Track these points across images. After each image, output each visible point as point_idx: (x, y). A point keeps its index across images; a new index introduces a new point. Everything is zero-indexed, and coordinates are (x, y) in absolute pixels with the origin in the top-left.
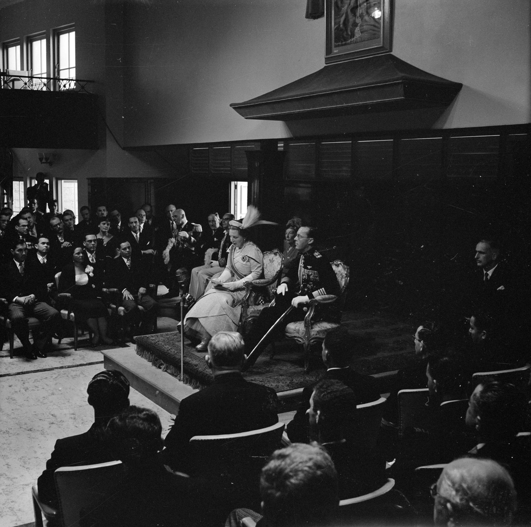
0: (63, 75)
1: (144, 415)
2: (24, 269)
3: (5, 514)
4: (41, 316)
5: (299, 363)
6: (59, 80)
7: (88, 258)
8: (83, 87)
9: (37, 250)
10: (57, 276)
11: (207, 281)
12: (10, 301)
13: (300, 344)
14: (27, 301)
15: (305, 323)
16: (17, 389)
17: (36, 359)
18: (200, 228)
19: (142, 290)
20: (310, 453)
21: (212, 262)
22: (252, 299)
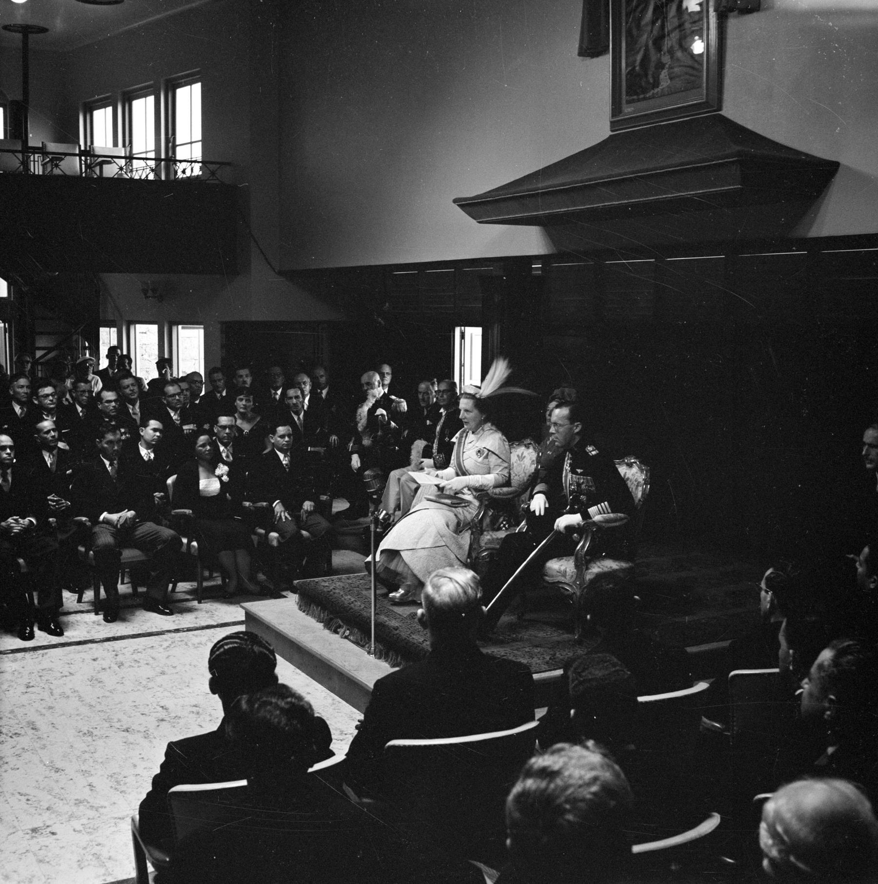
0: (182, 153)
2: (118, 471)
4: (147, 544)
6: (175, 161)
10: (170, 481)
12: (95, 521)
14: (122, 521)
16: (105, 664)
18: (404, 406)
19: (308, 505)
22: (487, 521)
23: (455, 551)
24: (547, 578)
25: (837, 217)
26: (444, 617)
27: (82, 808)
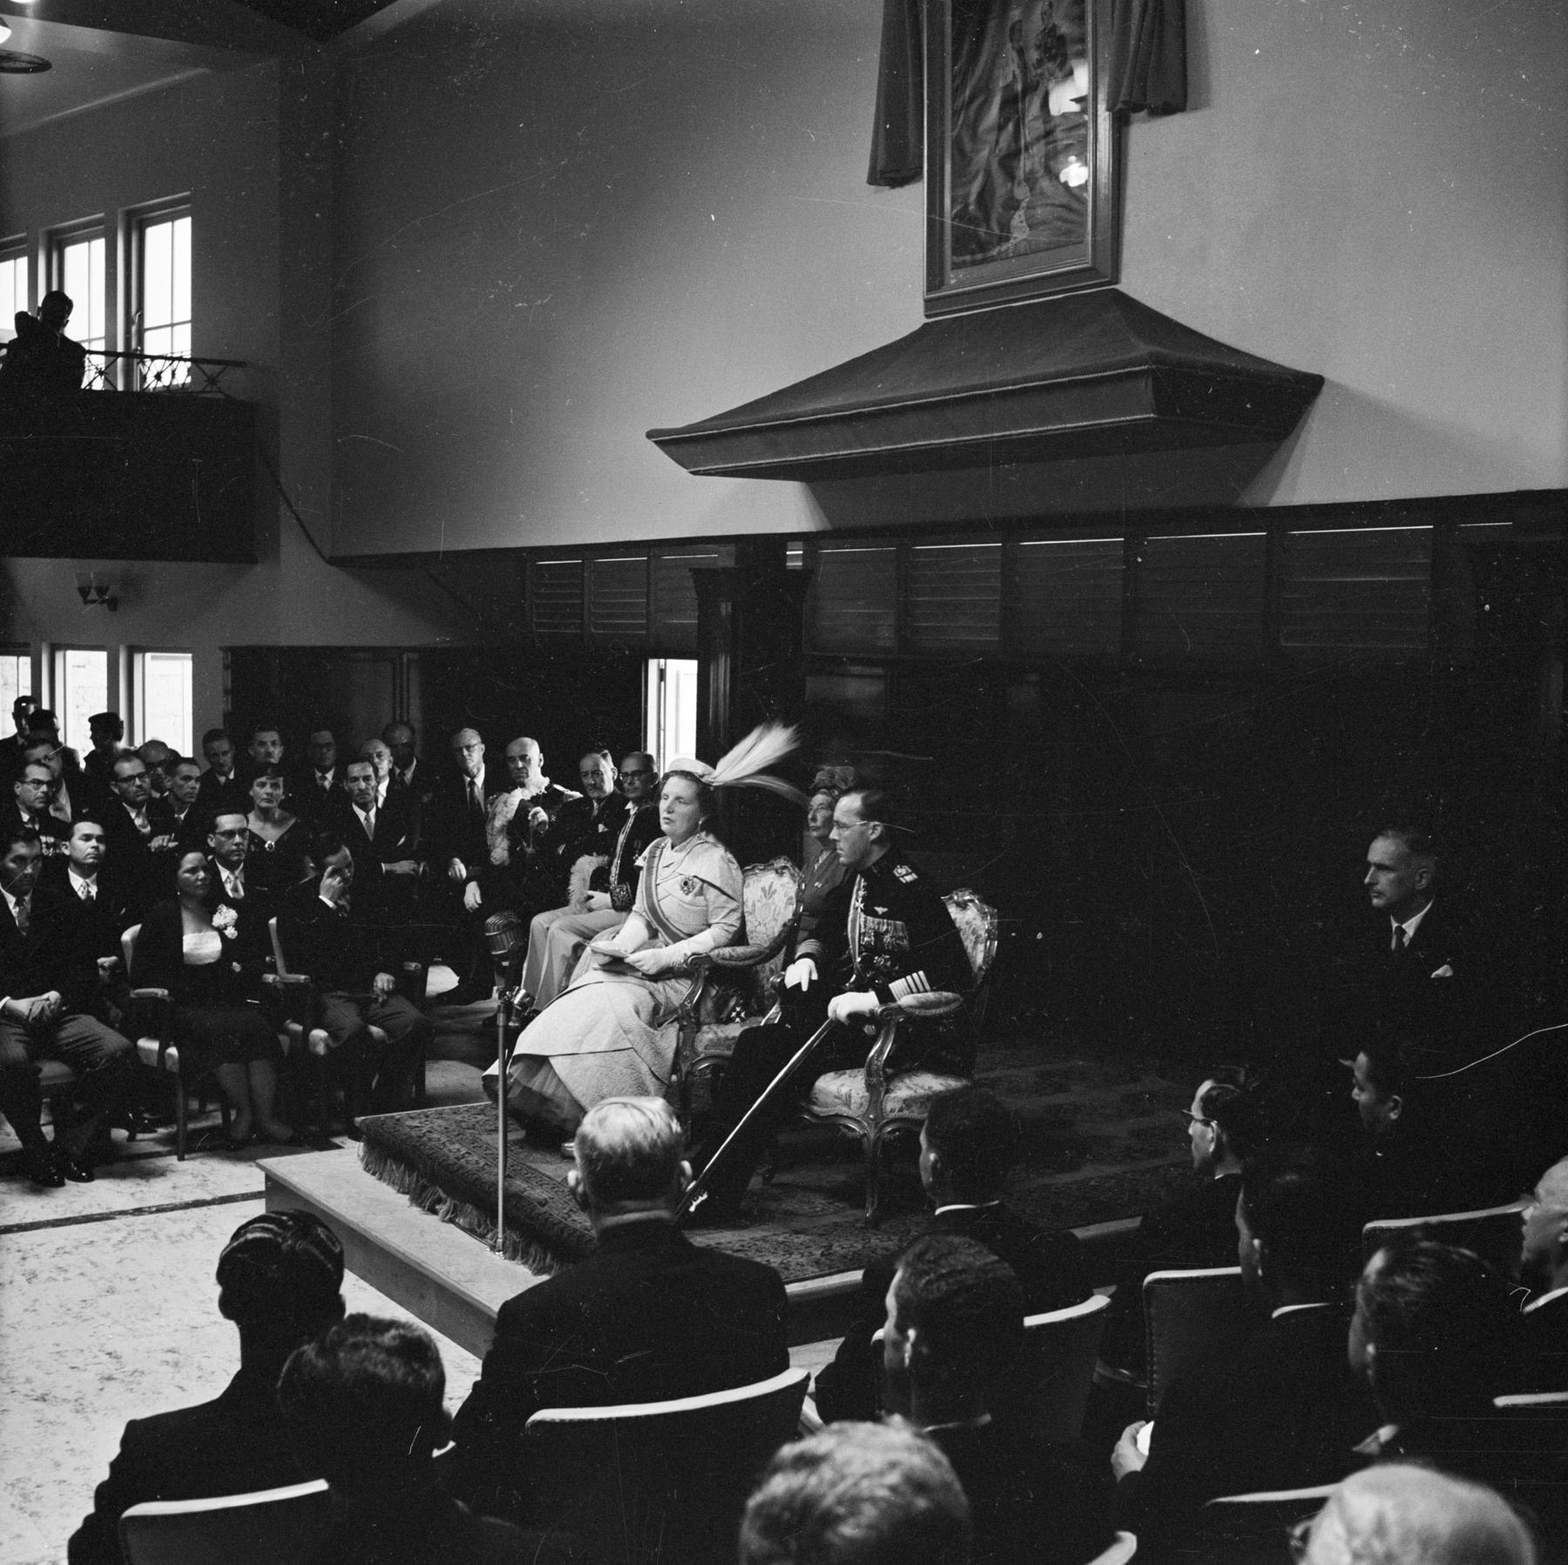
0: (154, 343)
1: (394, 1338)
4: (78, 1055)
5: (849, 1195)
6: (142, 357)
7: (221, 885)
8: (212, 380)
9: (66, 861)
10: (127, 936)
11: (578, 949)
13: (854, 1139)
14: (36, 1010)
15: (869, 1074)
17: (62, 1184)
19: (383, 981)
20: (890, 1448)
21: (591, 897)
22: (709, 1004)
26: (619, 1174)
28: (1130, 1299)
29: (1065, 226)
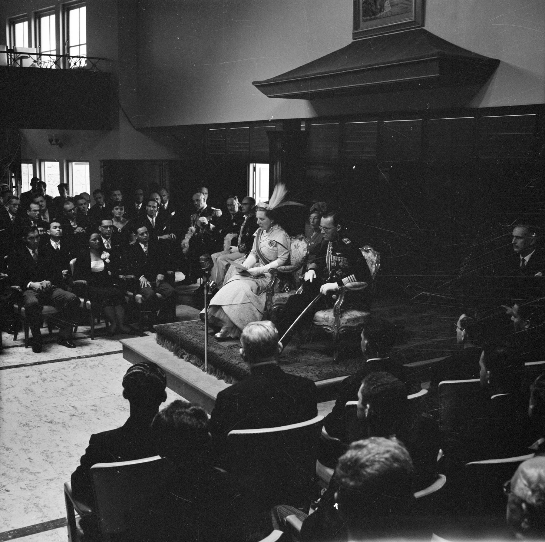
0: (73, 52)
1: (192, 410)
2: (39, 256)
3: (30, 510)
4: (59, 303)
6: (69, 57)
7: (103, 244)
8: (94, 65)
10: (72, 262)
11: (228, 266)
15: (335, 311)
16: (34, 380)
18: (220, 213)
19: (160, 277)
21: (231, 248)
22: (277, 286)
23: (256, 306)
24: (316, 323)
25: (498, 95)
26: (258, 349)
27: (25, 473)
28: (433, 392)
29: (405, 6)
